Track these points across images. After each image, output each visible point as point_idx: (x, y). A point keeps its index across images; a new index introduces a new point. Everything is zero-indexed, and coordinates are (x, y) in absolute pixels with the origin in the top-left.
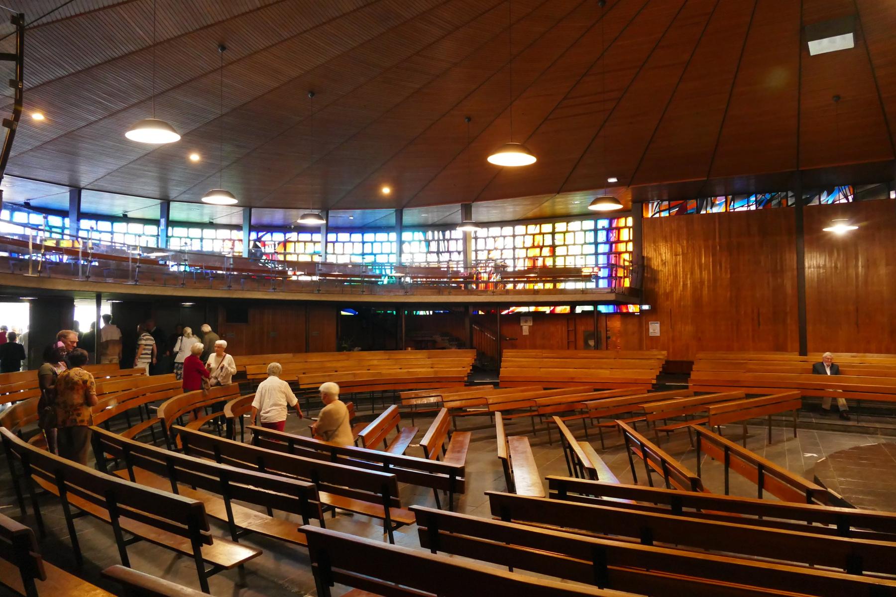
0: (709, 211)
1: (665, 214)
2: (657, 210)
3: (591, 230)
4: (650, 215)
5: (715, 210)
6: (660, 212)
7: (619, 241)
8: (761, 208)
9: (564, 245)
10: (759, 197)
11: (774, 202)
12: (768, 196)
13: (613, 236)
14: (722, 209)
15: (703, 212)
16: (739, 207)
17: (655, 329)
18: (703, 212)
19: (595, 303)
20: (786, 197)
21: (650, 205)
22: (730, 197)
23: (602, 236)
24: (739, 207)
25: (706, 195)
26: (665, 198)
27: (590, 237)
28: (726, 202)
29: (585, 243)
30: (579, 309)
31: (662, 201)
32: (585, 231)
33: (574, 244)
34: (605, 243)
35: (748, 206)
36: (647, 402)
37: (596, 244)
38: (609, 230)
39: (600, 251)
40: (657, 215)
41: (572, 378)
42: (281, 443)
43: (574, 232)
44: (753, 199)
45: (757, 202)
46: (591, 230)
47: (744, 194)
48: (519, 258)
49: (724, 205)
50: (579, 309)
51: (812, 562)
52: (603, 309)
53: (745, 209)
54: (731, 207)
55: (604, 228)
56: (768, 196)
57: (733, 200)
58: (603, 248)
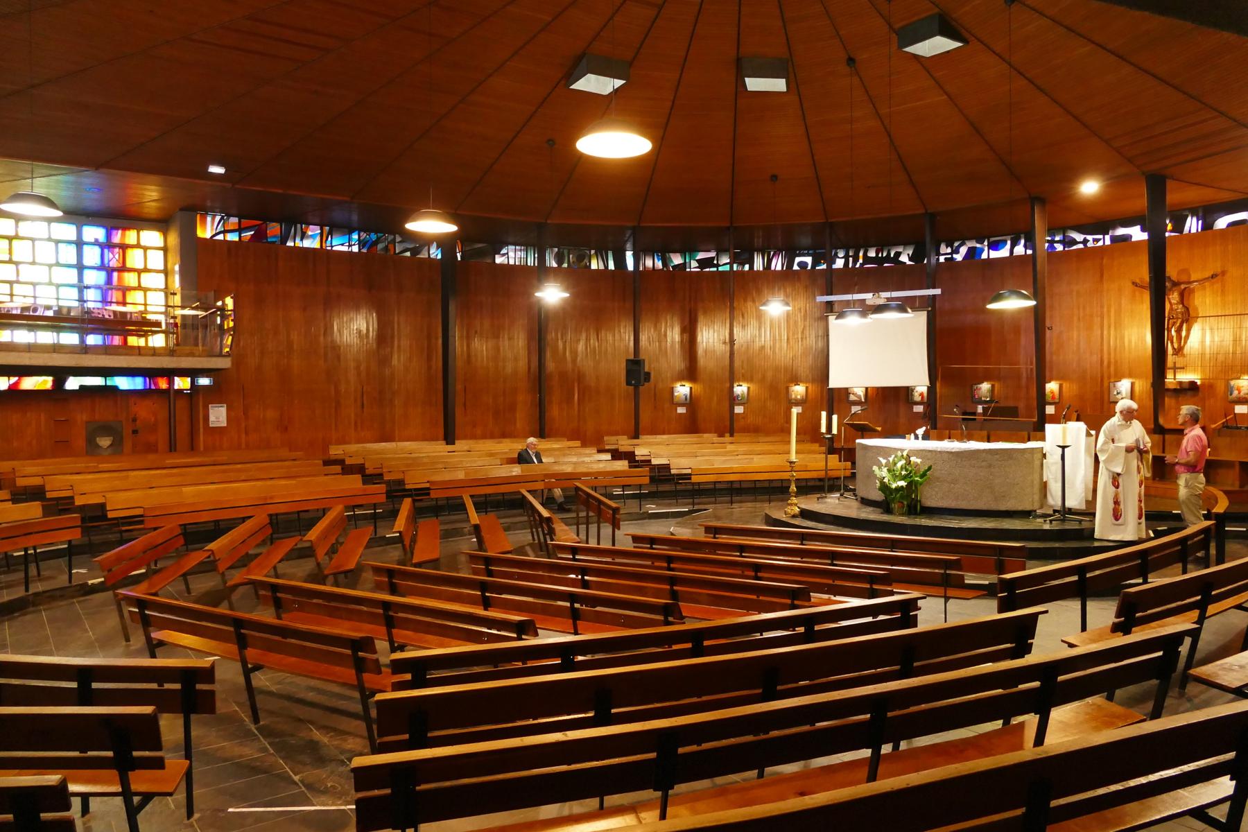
0: (299, 243)
1: (232, 237)
2: (220, 228)
3: (70, 242)
4: (208, 235)
5: (307, 243)
6: (224, 232)
7: (123, 269)
8: (364, 250)
9: (10, 261)
10: (364, 235)
11: (380, 246)
12: (374, 237)
13: (113, 259)
14: (316, 244)
15: (290, 244)
16: (339, 244)
17: (218, 415)
18: (290, 244)
19: (60, 374)
20: (394, 241)
21: (209, 219)
22: (327, 228)
23: (92, 256)
24: (339, 244)
25: (295, 220)
26: (233, 212)
27: (69, 254)
28: (321, 234)
29: (58, 264)
30: (73, 383)
31: (229, 215)
32: (57, 242)
33: (33, 263)
34: (98, 269)
35: (350, 246)
36: (130, 524)
37: (80, 267)
38: (107, 245)
39: (87, 282)
40: (220, 237)
41: (266, 498)
42: (774, 733)
43: (33, 240)
44: (355, 236)
45: (361, 243)
46: (70, 242)
47: (347, 229)
48: (88, 287)
49: (318, 239)
50: (73, 383)
51: (836, 621)
52: (123, 383)
53: (345, 249)
54: (328, 243)
55: (96, 243)
56: (374, 237)
57: (330, 233)
58: (97, 278)
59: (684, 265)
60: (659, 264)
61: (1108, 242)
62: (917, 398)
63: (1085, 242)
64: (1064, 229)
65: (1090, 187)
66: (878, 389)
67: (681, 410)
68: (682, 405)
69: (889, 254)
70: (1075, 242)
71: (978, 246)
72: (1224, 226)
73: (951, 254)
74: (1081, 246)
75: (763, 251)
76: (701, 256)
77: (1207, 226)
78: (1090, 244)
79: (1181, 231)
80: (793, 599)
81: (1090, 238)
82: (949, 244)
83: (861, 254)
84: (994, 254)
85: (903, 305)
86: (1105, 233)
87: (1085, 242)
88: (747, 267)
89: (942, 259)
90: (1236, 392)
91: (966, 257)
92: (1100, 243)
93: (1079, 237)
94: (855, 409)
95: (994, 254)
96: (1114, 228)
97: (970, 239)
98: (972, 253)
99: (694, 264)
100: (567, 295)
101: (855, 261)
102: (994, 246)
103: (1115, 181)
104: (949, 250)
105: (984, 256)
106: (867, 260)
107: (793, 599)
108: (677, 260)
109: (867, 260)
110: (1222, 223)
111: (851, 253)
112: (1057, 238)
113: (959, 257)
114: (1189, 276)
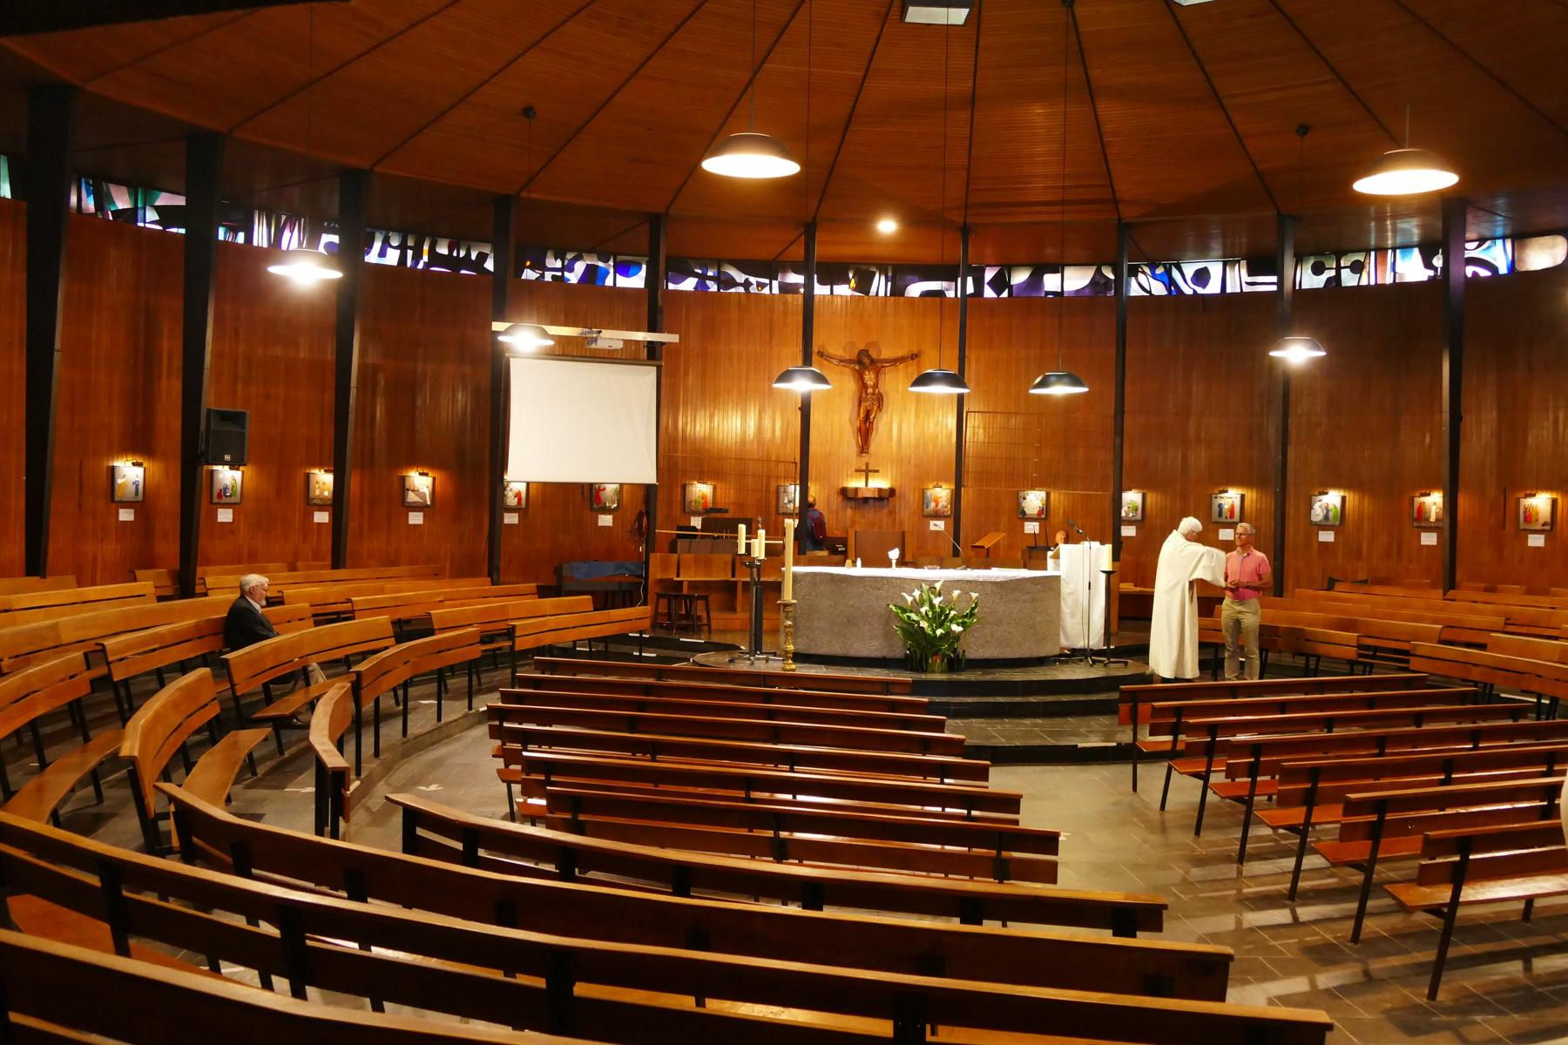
59: (131, 215)
60: (89, 204)
61: (776, 290)
62: (511, 501)
63: (747, 284)
64: (719, 263)
65: (887, 226)
66: (545, 485)
67: (126, 515)
68: (127, 504)
69: (468, 254)
70: (732, 283)
71: (601, 264)
72: (917, 294)
73: (562, 270)
74: (741, 290)
75: (270, 213)
76: (164, 199)
77: (898, 291)
78: (753, 289)
79: (867, 293)
80: (575, 811)
81: (753, 280)
82: (560, 255)
83: (426, 248)
84: (623, 282)
85: (628, 356)
86: (773, 277)
87: (747, 284)
88: (241, 238)
89: (548, 276)
90: (933, 505)
91: (582, 279)
92: (766, 291)
93: (740, 277)
94: (416, 518)
95: (623, 282)
96: (785, 271)
97: (590, 251)
98: (591, 274)
99: (152, 215)
100: (337, 275)
101: (417, 257)
102: (623, 269)
103: (914, 218)
104: (558, 264)
105: (609, 282)
106: (435, 258)
107: (575, 811)
108: (122, 202)
109: (435, 258)
110: (915, 289)
111: (411, 243)
112: (710, 273)
113: (573, 278)
114: (880, 352)
